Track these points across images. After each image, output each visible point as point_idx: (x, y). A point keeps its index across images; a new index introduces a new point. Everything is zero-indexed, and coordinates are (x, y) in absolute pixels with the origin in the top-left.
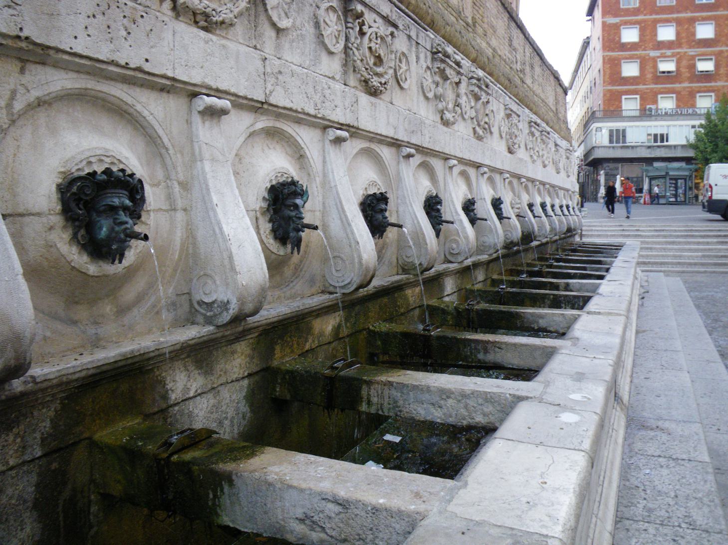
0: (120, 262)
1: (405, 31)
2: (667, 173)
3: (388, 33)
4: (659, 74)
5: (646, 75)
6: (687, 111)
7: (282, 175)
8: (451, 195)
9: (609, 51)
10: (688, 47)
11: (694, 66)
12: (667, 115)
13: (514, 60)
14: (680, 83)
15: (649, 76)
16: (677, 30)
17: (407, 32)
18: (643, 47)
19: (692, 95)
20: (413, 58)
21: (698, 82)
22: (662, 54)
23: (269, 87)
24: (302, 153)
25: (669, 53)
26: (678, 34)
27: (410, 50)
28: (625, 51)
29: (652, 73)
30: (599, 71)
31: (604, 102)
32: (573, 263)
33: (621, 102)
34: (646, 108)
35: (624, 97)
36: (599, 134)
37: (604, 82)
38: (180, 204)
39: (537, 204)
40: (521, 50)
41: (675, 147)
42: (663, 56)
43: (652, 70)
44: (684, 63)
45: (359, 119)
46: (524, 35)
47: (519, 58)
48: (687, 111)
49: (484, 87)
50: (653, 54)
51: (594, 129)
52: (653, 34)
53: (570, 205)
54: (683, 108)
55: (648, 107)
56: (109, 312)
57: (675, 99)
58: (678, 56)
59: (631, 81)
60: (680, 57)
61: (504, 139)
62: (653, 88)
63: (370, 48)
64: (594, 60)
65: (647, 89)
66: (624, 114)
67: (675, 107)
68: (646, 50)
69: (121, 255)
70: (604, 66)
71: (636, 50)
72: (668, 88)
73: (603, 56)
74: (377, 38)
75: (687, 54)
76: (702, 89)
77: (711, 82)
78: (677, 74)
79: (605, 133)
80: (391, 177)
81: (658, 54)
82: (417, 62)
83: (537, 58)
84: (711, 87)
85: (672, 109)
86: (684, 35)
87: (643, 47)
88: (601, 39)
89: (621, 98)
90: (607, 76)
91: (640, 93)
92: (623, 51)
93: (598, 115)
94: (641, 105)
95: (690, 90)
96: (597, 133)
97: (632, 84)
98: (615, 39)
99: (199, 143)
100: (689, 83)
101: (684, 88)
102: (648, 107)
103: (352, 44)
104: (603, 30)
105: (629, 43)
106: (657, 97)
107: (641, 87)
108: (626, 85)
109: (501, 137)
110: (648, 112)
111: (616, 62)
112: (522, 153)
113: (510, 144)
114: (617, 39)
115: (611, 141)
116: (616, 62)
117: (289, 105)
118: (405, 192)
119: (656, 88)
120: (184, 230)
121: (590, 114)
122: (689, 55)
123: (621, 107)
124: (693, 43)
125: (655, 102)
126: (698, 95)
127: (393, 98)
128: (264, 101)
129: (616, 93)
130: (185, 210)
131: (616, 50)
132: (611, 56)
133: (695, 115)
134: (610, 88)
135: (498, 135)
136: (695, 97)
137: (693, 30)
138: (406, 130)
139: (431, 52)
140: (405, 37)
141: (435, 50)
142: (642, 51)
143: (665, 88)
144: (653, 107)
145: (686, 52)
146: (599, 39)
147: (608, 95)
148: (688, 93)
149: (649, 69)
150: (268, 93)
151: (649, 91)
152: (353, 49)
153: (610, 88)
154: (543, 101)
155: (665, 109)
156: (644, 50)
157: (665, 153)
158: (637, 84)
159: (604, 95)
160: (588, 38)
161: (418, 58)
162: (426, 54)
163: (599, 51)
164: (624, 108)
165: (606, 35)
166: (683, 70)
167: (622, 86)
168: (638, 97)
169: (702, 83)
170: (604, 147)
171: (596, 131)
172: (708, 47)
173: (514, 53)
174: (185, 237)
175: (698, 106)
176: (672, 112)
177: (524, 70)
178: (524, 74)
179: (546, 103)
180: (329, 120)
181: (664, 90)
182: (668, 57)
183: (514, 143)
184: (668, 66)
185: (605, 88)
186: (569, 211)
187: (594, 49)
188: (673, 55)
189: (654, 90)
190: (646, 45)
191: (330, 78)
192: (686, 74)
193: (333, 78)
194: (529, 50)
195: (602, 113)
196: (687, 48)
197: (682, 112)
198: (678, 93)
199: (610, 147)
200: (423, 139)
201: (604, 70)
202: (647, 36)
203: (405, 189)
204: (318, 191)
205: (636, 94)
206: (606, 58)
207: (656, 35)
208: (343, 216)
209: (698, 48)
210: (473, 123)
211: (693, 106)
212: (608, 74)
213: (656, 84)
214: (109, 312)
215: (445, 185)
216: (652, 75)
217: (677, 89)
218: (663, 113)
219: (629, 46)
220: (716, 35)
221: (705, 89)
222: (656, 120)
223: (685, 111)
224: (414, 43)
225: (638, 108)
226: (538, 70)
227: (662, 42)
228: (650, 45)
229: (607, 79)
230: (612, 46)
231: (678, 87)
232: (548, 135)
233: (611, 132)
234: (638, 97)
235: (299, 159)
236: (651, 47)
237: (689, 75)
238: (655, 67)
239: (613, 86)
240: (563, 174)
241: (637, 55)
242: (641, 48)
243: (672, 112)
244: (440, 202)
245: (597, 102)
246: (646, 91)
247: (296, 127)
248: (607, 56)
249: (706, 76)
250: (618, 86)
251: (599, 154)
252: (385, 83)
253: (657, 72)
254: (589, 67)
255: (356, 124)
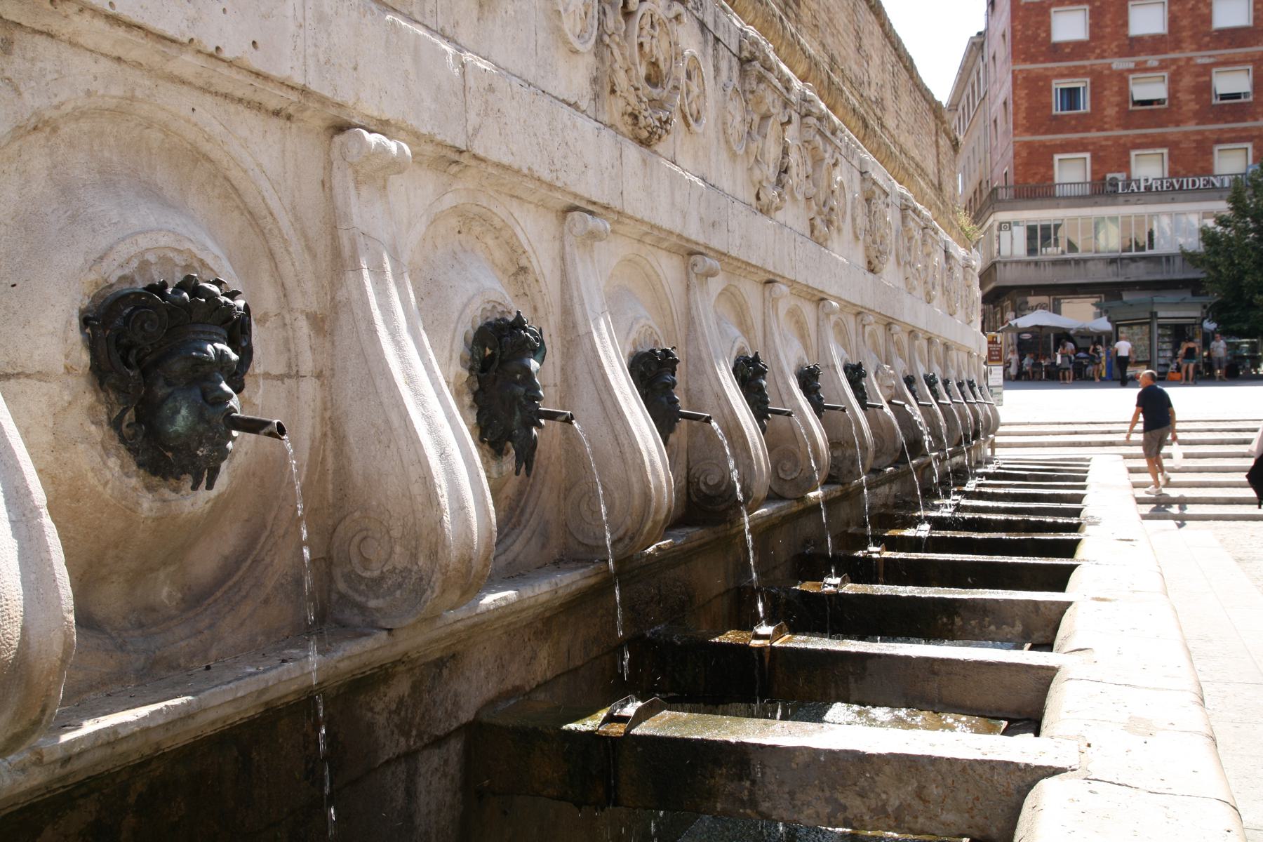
0: (210, 486)
1: (695, 12)
2: (1154, 315)
3: (672, 14)
4: (1131, 107)
5: (1104, 109)
6: (1194, 183)
7: (494, 307)
8: (777, 356)
9: (1025, 61)
10: (1194, 47)
11: (1207, 87)
12: (1150, 193)
13: (866, 79)
14: (1177, 124)
15: (1111, 111)
16: (1170, 12)
17: (699, 15)
18: (1098, 51)
19: (1204, 149)
20: (708, 70)
21: (1217, 121)
22: (1137, 64)
23: (473, 119)
24: (523, 262)
25: (1153, 61)
26: (1173, 21)
27: (704, 54)
28: (1060, 61)
29: (1118, 105)
30: (1005, 103)
31: (1016, 168)
32: (1070, 481)
33: (1051, 167)
34: (1104, 178)
35: (1057, 157)
36: (1005, 235)
37: (1015, 127)
38: (307, 363)
39: (920, 378)
40: (876, 60)
41: (1169, 258)
42: (1141, 68)
43: (1116, 99)
44: (1187, 81)
45: (625, 193)
46: (882, 26)
47: (873, 75)
48: (1194, 183)
49: (828, 134)
50: (1119, 64)
51: (996, 224)
52: (1120, 22)
53: (975, 382)
54: (1185, 176)
55: (1109, 176)
56: (167, 602)
57: (1166, 157)
58: (1174, 67)
59: (1073, 122)
60: (1179, 67)
61: (861, 242)
62: (1120, 137)
63: (641, 45)
64: (992, 80)
65: (1107, 138)
66: (1058, 191)
67: (1166, 175)
68: (1103, 58)
69: (205, 473)
70: (1014, 93)
71: (1083, 57)
72: (1152, 135)
73: (1013, 72)
74: (652, 26)
75: (1192, 63)
76: (1227, 135)
77: (1245, 121)
78: (1171, 104)
79: (1020, 234)
80: (675, 317)
81: (1132, 66)
82: (715, 78)
83: (904, 75)
84: (1245, 129)
85: (1162, 180)
86: (1185, 22)
87: (1098, 51)
88: (1008, 36)
89: (1052, 159)
90: (1022, 115)
91: (1091, 147)
92: (1054, 61)
93: (1002, 194)
94: (1094, 172)
95: (1199, 137)
96: (1001, 233)
97: (1075, 130)
98: (1039, 35)
99: (351, 232)
100: (1197, 124)
101: (1186, 134)
102: (1109, 176)
103: (610, 36)
104: (1014, 17)
105: (1067, 44)
106: (1128, 156)
107: (1093, 134)
108: (1061, 132)
109: (857, 238)
110: (1109, 188)
111: (1041, 84)
112: (890, 273)
113: (873, 254)
114: (1043, 35)
115: (1032, 250)
116: (1041, 84)
117: (506, 160)
118: (702, 348)
119: (1127, 136)
120: (318, 419)
121: (985, 195)
122: (1197, 65)
123: (1052, 179)
124: (1207, 39)
125: (1125, 166)
126: (1216, 148)
127: (678, 150)
128: (465, 149)
129: (1041, 149)
130: (319, 376)
131: (1041, 59)
132: (1028, 71)
133: (1211, 191)
134: (1028, 138)
135: (851, 236)
136: (1212, 153)
137: (1205, 11)
138: (701, 219)
139: (739, 59)
140: (696, 25)
141: (745, 54)
142: (1097, 58)
143: (1145, 136)
144: (1121, 176)
145: (1190, 59)
146: (1004, 36)
147: (1024, 154)
148: (1194, 145)
149: (1111, 96)
150: (471, 132)
151: (1110, 143)
152: (614, 47)
153: (1028, 138)
154: (917, 165)
155: (1147, 180)
156: (1101, 56)
157: (1148, 273)
158: (1087, 129)
159: (1016, 155)
160: (979, 34)
161: (717, 69)
162: (730, 61)
163: (1005, 62)
164: (1057, 180)
165: (1020, 27)
166: (1182, 96)
167: (1054, 133)
168: (1087, 155)
169: (1226, 122)
170: (1018, 262)
171: (1000, 229)
172: (1238, 47)
173: (866, 65)
174: (318, 434)
175: (1217, 172)
176: (1162, 185)
177: (882, 100)
178: (883, 109)
179: (923, 170)
180: (576, 196)
181: (1144, 140)
182: (1153, 69)
183: (879, 251)
184: (1150, 88)
185: (1017, 139)
186: (974, 393)
187: (994, 58)
188: (1162, 66)
189: (1122, 141)
190: (1105, 47)
191: (570, 105)
192: (1190, 104)
193: (575, 106)
194: (891, 58)
195: (1011, 192)
196: (1192, 50)
197: (1181, 186)
198: (1172, 145)
199: (1029, 263)
200: (730, 239)
201: (1014, 102)
202: (1107, 26)
203: (701, 342)
204: (551, 342)
205: (1085, 150)
206: (1020, 77)
207: (1126, 24)
208: (605, 396)
209: (1216, 49)
210: (809, 208)
211: (1208, 171)
212: (1023, 108)
213: (1126, 127)
214: (167, 602)
215: (765, 336)
216: (1117, 109)
217: (1171, 138)
218: (1142, 189)
219: (1067, 50)
220: (1256, 18)
221: (1233, 135)
222: (1127, 202)
223: (1187, 182)
224: (710, 38)
225: (1089, 179)
226: (906, 101)
227: (1139, 40)
228: (1113, 45)
229: (1022, 121)
230: (1033, 50)
231: (1172, 133)
232: (934, 236)
233: (1031, 231)
234: (1087, 155)
235: (516, 275)
236: (1115, 50)
237: (1197, 107)
238: (1124, 91)
239: (1033, 134)
240: (959, 320)
241: (1084, 67)
242: (1093, 52)
243: (1162, 185)
244: (762, 372)
245: (1002, 166)
246: (1104, 143)
247: (514, 206)
248: (1021, 71)
249: (1233, 107)
250: (1045, 133)
251: (1008, 277)
252: (666, 122)
253: (1127, 102)
254: (982, 95)
255: (616, 204)
